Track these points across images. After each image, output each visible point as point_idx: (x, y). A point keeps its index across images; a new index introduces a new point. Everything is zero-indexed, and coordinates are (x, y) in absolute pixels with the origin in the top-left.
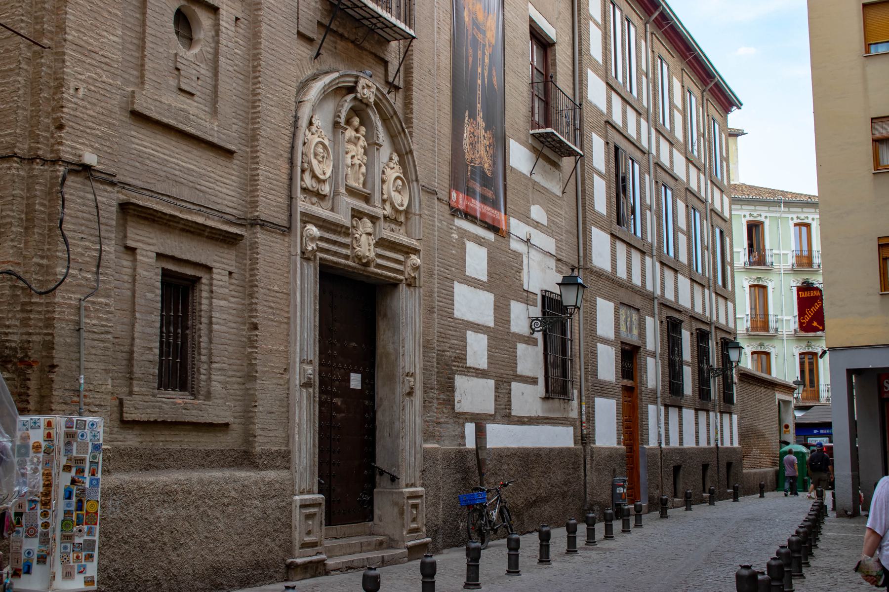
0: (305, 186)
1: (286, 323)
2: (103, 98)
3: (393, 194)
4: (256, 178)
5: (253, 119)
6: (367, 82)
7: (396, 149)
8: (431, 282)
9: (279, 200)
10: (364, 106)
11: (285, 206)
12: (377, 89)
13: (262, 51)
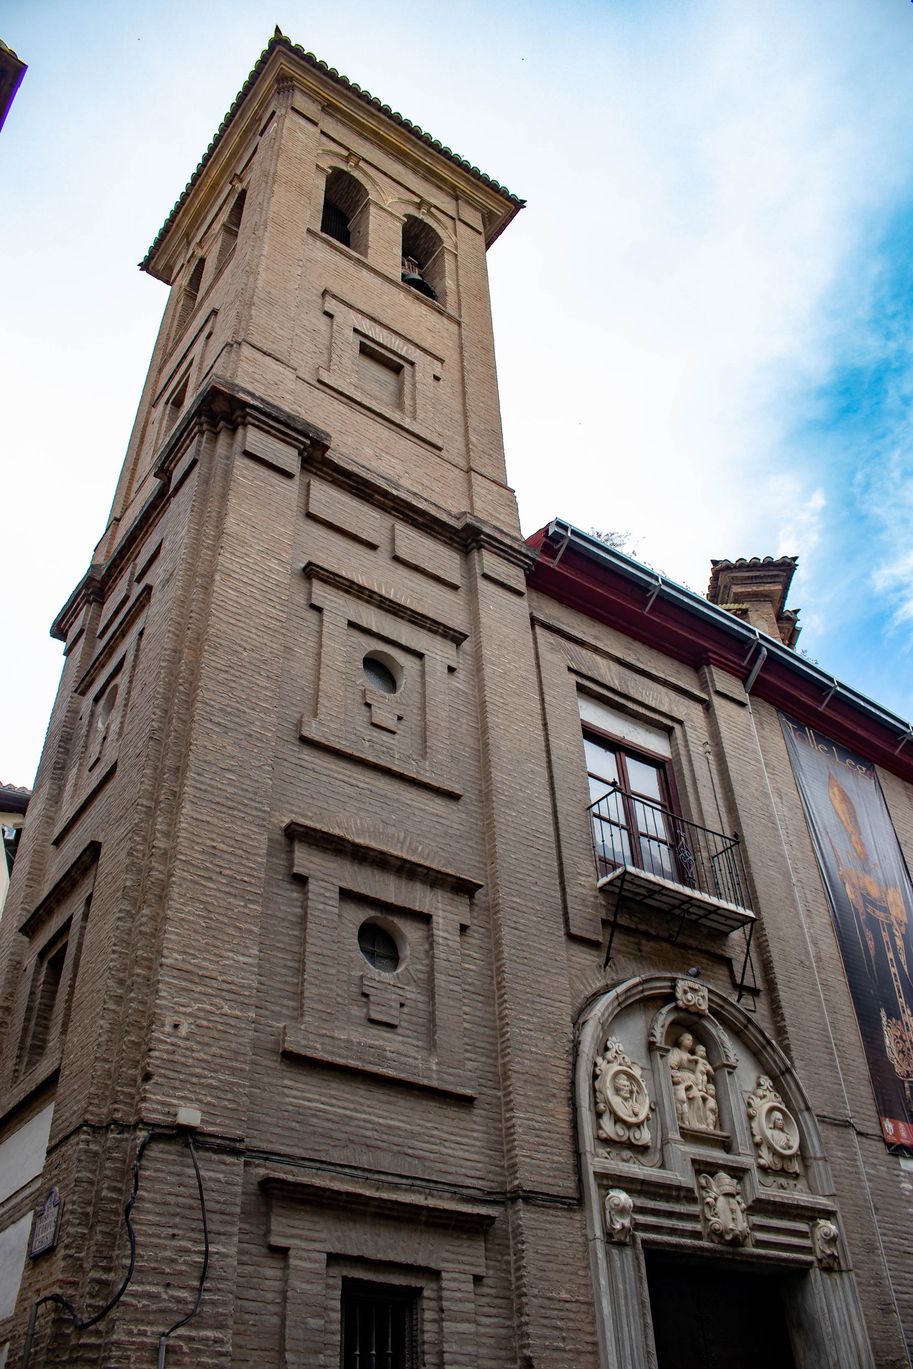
0: (604, 1135)
1: (590, 1353)
2: (222, 1035)
3: (769, 1133)
4: (512, 1130)
5: (502, 1050)
6: (691, 984)
7: (764, 1067)
8: (874, 1261)
9: (556, 1158)
10: (695, 1018)
11: (571, 1167)
12: (710, 991)
13: (504, 961)
